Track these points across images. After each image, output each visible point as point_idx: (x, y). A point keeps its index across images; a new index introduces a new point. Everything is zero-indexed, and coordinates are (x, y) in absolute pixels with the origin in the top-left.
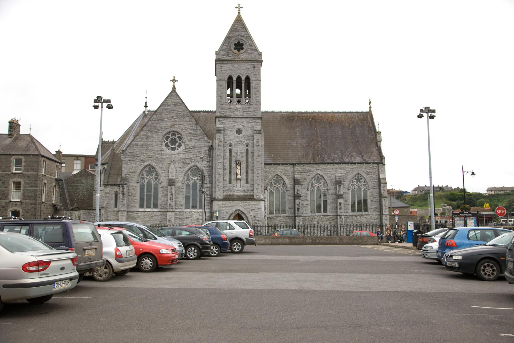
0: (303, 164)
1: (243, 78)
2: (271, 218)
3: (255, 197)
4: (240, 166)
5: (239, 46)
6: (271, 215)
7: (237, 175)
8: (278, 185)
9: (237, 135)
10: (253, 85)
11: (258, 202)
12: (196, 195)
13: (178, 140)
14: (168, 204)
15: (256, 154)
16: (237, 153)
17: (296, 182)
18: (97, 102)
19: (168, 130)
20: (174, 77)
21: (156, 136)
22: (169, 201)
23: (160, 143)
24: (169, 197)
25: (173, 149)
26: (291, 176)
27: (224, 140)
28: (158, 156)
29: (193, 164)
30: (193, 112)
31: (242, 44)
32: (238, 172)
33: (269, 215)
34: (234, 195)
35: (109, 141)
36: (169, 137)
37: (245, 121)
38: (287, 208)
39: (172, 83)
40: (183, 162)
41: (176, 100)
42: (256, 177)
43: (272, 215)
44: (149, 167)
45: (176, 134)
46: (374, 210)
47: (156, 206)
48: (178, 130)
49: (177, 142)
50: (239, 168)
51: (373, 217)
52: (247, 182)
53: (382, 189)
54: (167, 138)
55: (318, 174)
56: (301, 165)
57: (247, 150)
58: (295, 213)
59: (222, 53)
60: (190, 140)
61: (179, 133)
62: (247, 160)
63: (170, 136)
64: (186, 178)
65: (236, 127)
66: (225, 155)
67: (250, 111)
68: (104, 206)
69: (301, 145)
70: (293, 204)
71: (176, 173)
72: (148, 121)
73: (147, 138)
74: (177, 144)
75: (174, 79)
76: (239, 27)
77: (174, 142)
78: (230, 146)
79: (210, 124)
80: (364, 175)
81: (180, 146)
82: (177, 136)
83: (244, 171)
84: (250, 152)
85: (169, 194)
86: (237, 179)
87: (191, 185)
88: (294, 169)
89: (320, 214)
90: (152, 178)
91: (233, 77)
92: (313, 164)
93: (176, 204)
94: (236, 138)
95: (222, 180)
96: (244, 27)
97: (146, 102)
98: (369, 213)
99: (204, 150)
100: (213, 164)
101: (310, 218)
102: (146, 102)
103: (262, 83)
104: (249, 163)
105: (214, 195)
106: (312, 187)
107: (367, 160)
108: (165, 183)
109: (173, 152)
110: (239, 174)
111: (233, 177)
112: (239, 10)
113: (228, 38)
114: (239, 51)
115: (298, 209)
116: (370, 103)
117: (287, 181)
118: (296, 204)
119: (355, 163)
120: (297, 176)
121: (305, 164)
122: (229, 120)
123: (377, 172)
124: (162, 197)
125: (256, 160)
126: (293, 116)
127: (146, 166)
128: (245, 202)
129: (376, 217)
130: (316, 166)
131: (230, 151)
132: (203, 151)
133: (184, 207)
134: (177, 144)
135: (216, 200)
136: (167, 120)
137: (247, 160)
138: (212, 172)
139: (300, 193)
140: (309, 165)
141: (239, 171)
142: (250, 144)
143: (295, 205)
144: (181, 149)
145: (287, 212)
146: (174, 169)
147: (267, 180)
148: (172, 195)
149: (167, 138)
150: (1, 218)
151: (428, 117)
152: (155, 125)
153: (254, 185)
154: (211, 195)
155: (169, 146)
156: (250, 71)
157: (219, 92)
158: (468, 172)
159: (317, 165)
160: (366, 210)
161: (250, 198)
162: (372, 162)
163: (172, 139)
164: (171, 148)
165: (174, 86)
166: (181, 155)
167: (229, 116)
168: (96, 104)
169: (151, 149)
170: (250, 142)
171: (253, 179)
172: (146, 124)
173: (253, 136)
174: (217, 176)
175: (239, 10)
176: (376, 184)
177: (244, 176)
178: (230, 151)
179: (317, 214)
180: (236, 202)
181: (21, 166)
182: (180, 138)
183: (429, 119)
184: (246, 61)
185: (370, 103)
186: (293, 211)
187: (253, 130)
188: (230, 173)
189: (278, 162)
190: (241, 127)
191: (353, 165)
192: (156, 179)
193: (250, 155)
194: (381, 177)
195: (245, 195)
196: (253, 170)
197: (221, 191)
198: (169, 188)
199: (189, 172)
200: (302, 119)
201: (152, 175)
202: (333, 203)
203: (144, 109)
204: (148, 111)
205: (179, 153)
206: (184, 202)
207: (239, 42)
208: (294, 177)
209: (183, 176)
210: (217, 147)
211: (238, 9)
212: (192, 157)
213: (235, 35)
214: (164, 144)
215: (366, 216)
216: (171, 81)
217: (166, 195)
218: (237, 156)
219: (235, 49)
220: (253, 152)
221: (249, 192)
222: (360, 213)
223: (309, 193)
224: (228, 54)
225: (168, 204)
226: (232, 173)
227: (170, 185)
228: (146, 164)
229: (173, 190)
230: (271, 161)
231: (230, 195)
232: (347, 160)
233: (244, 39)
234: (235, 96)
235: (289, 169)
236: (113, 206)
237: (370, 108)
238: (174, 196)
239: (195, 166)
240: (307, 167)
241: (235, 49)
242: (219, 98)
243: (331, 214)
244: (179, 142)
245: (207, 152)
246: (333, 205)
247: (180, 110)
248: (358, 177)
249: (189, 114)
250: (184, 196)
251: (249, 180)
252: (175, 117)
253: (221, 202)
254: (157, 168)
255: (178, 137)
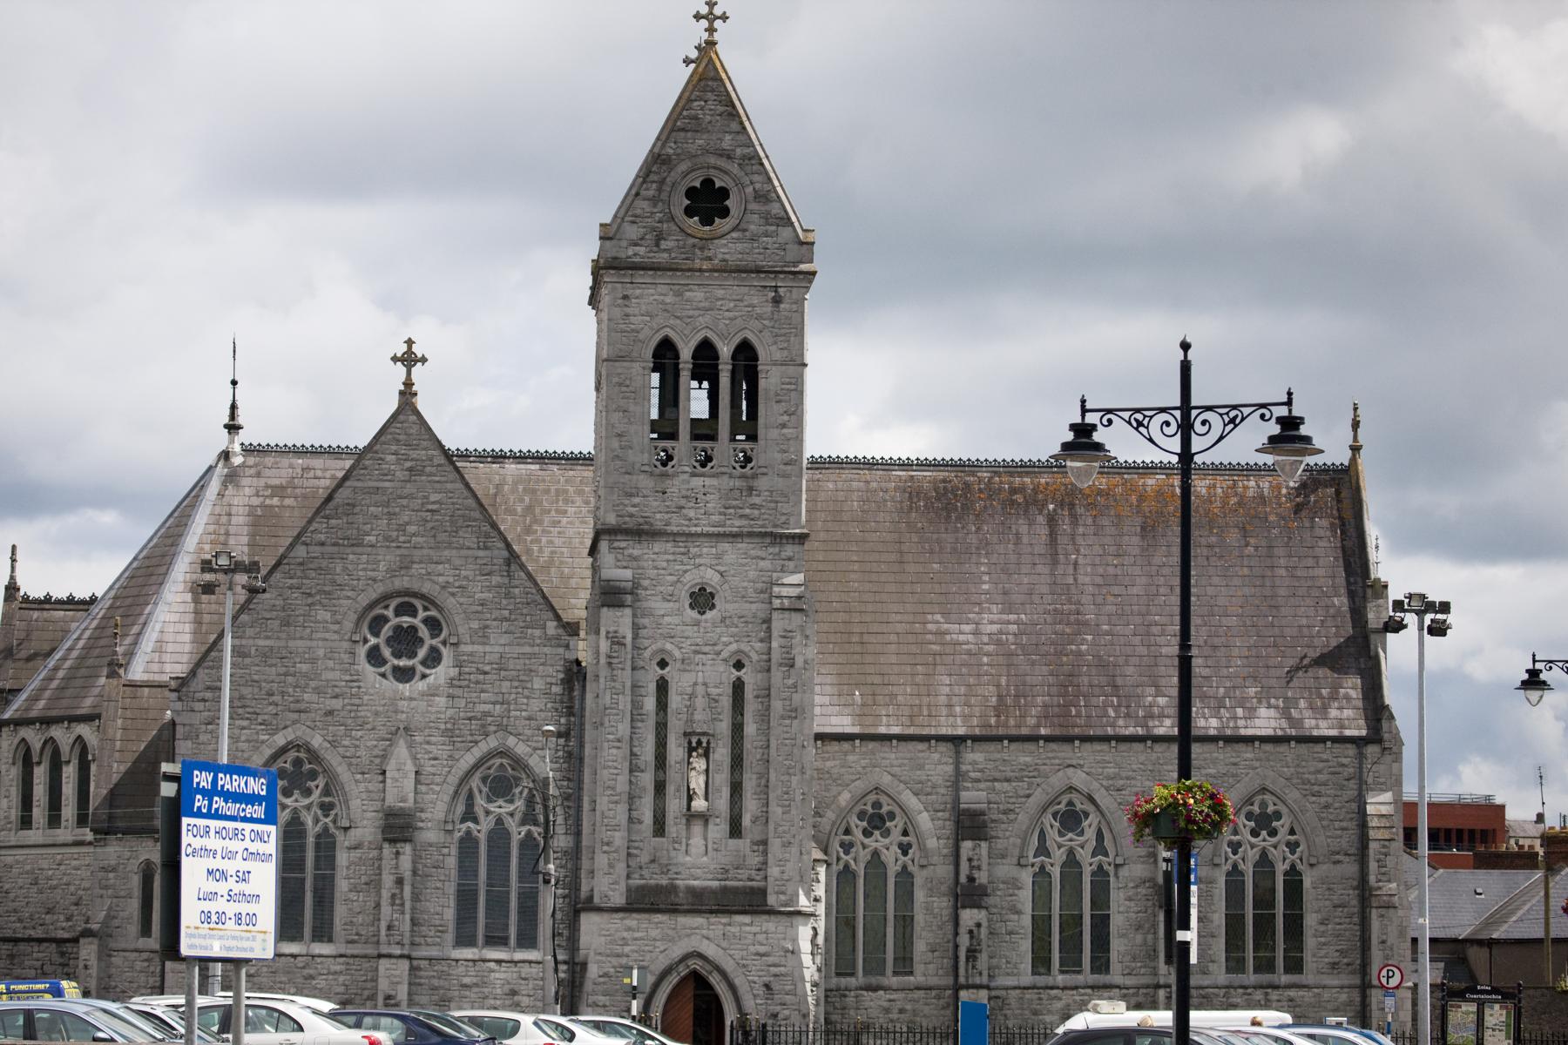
0: (999, 739)
1: (725, 351)
2: (841, 992)
3: (772, 900)
4: (706, 755)
5: (708, 202)
6: (844, 981)
7: (690, 799)
8: (876, 841)
9: (694, 614)
10: (769, 381)
11: (784, 919)
12: (506, 881)
13: (424, 632)
14: (383, 925)
15: (777, 706)
16: (692, 696)
17: (969, 825)
18: (211, 570)
19: (380, 589)
20: (410, 342)
21: (328, 616)
22: (386, 910)
23: (346, 645)
24: (385, 894)
25: (404, 675)
26: (943, 795)
27: (636, 637)
28: (336, 704)
29: (492, 742)
30: (465, 455)
31: (724, 193)
32: (697, 783)
33: (835, 981)
34: (672, 889)
35: (48, 599)
36: (386, 620)
37: (732, 553)
38: (920, 947)
39: (401, 369)
40: (449, 734)
41: (417, 447)
42: (776, 810)
43: (852, 981)
44: (292, 754)
45: (418, 603)
46: (1334, 965)
47: (323, 932)
48: (426, 588)
49: (413, 629)
50: (699, 764)
51: (1326, 995)
52: (735, 830)
53: (1373, 866)
54: (377, 624)
55: (1071, 789)
56: (992, 746)
57: (738, 687)
58: (956, 976)
59: (632, 232)
60: (482, 636)
61: (429, 601)
62: (737, 729)
63: (390, 613)
64: (460, 808)
65: (692, 579)
66: (636, 705)
67: (753, 506)
68: (95, 927)
69: (999, 643)
70: (949, 928)
71: (417, 782)
72: (292, 546)
73: (286, 623)
74: (422, 653)
75: (409, 351)
76: (707, 111)
77: (405, 641)
78: (663, 664)
79: (556, 523)
80: (1292, 795)
81: (434, 658)
82: (421, 614)
83: (722, 779)
84: (749, 693)
85: (388, 880)
86: (691, 816)
87: (482, 837)
88: (957, 764)
89: (1080, 979)
90: (308, 807)
91: (680, 345)
92: (1048, 739)
93: (414, 923)
94: (689, 631)
95: (622, 818)
96: (730, 111)
97: (233, 407)
98: (1308, 977)
99: (547, 678)
100: (582, 746)
101: (1029, 995)
102: (233, 407)
103: (809, 374)
104: (747, 745)
105: (584, 889)
106: (1043, 850)
107: (1309, 723)
108: (367, 828)
109: (405, 689)
110: (700, 791)
111: (674, 805)
112: (711, 30)
113: (657, 162)
114: (706, 221)
115: (972, 954)
116: (1356, 409)
117: (924, 821)
118: (963, 930)
119: (1250, 740)
120: (972, 797)
121: (1013, 739)
122: (657, 547)
123: (1353, 784)
124: (354, 889)
125: (776, 731)
126: (967, 485)
127: (283, 751)
128: (724, 920)
129: (1344, 997)
130: (1064, 752)
131: (662, 687)
132: (538, 684)
133: (450, 937)
134: (422, 653)
135: (599, 910)
136: (361, 534)
137: (737, 729)
138: (580, 782)
139: (982, 877)
140: (1030, 746)
141: (702, 779)
142: (755, 657)
143: (956, 934)
144: (442, 673)
145: (918, 968)
146: (410, 767)
147: (831, 815)
148: (400, 882)
149: (377, 624)
150: (1, 987)
151: (1421, 629)
152: (324, 563)
153: (765, 843)
154: (572, 882)
155: (384, 662)
156: (759, 317)
157: (616, 416)
158: (1234, 416)
159: (1066, 747)
160: (1295, 965)
161: (747, 900)
162: (1334, 733)
163: (398, 629)
164: (396, 669)
165: (408, 384)
166: (441, 701)
167: (659, 525)
168: (208, 577)
169: (305, 675)
170: (753, 649)
171: (764, 818)
172: (283, 556)
173: (768, 621)
174: (603, 803)
175: (711, 30)
176: (1348, 840)
177: (722, 803)
178: (662, 687)
179: (1060, 979)
180: (684, 920)
181: (54, 820)
182: (434, 625)
183: (1427, 637)
184: (739, 270)
185: (1356, 409)
186: (947, 962)
187: (767, 590)
188: (660, 788)
189: (883, 730)
190: (711, 577)
191: (1241, 747)
192: (326, 808)
193: (751, 706)
194: (1370, 809)
195: (725, 890)
196: (764, 776)
197: (621, 868)
198: (388, 850)
199: (475, 782)
200: (1013, 503)
201: (307, 792)
202: (1139, 927)
203: (222, 440)
204: (248, 450)
205: (432, 693)
206: (450, 914)
207: (708, 182)
208: (957, 800)
209: (447, 798)
210: (604, 672)
211: (704, 23)
212: (486, 714)
213: (692, 148)
214: (362, 651)
215: (1292, 993)
216: (395, 359)
217: (375, 884)
218: (691, 708)
219: (689, 212)
220: (766, 694)
221: (744, 874)
222: (1265, 978)
223: (1026, 877)
224: (659, 238)
225: (383, 925)
226: (670, 789)
227: (392, 841)
228: (280, 740)
229: (406, 862)
230: (847, 720)
231: (658, 889)
232: (1214, 722)
233: (734, 168)
234: (684, 430)
235: (938, 764)
236: (134, 928)
237: (1355, 449)
238: (407, 889)
239: (502, 754)
240: (1023, 756)
241: (689, 212)
242: (615, 444)
243: (1129, 981)
244: (429, 642)
245: (556, 689)
246: (1139, 938)
247: (434, 497)
248: (1263, 805)
249: (477, 515)
250: (451, 889)
251: (746, 820)
252: (412, 529)
253: (616, 923)
254: (333, 759)
255: (426, 621)
